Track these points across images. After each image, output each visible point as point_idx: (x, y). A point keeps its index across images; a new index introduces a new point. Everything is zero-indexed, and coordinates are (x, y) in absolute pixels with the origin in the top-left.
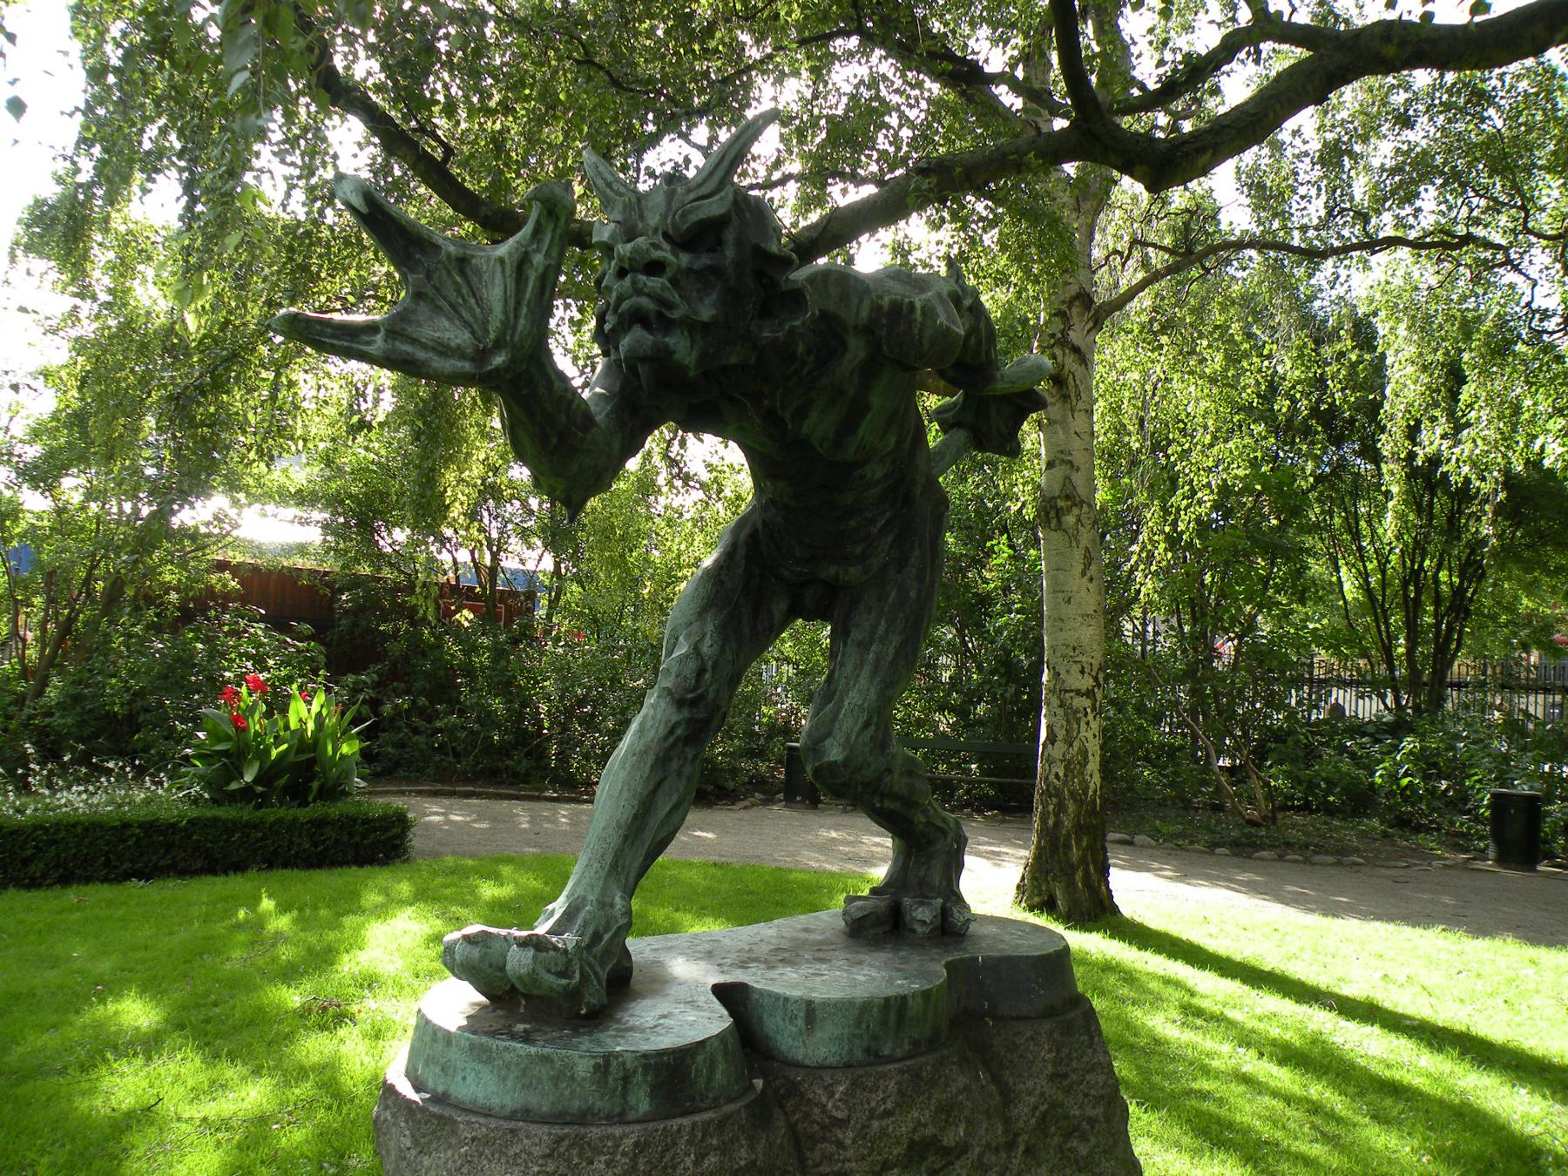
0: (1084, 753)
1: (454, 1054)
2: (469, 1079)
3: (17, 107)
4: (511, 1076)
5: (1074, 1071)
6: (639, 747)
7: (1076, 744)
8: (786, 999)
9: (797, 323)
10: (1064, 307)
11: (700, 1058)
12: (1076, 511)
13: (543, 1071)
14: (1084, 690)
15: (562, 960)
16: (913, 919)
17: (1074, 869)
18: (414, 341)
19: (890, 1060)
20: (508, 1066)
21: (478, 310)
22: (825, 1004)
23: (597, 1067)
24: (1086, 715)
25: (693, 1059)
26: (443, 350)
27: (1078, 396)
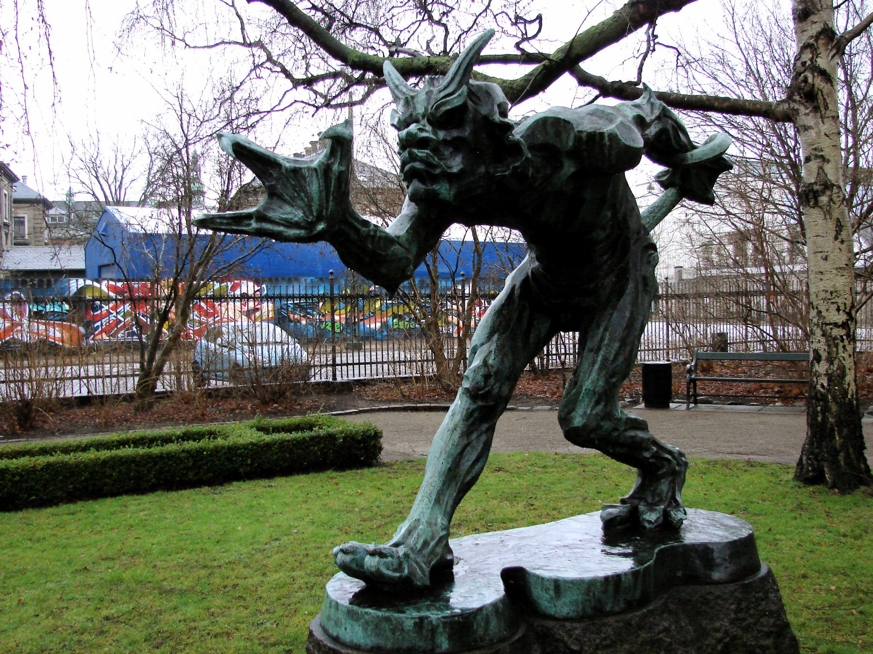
0: (842, 369)
1: (341, 615)
2: (348, 630)
4: (369, 628)
5: (752, 616)
6: (451, 426)
7: (836, 362)
8: (543, 579)
9: (518, 164)
10: (812, 41)
11: (479, 617)
12: (828, 193)
13: (386, 626)
14: (840, 323)
15: (396, 562)
16: (644, 519)
17: (837, 452)
19: (612, 613)
20: (367, 623)
22: (566, 581)
23: (415, 623)
24: (842, 341)
25: (474, 618)
26: (290, 224)
27: (826, 107)
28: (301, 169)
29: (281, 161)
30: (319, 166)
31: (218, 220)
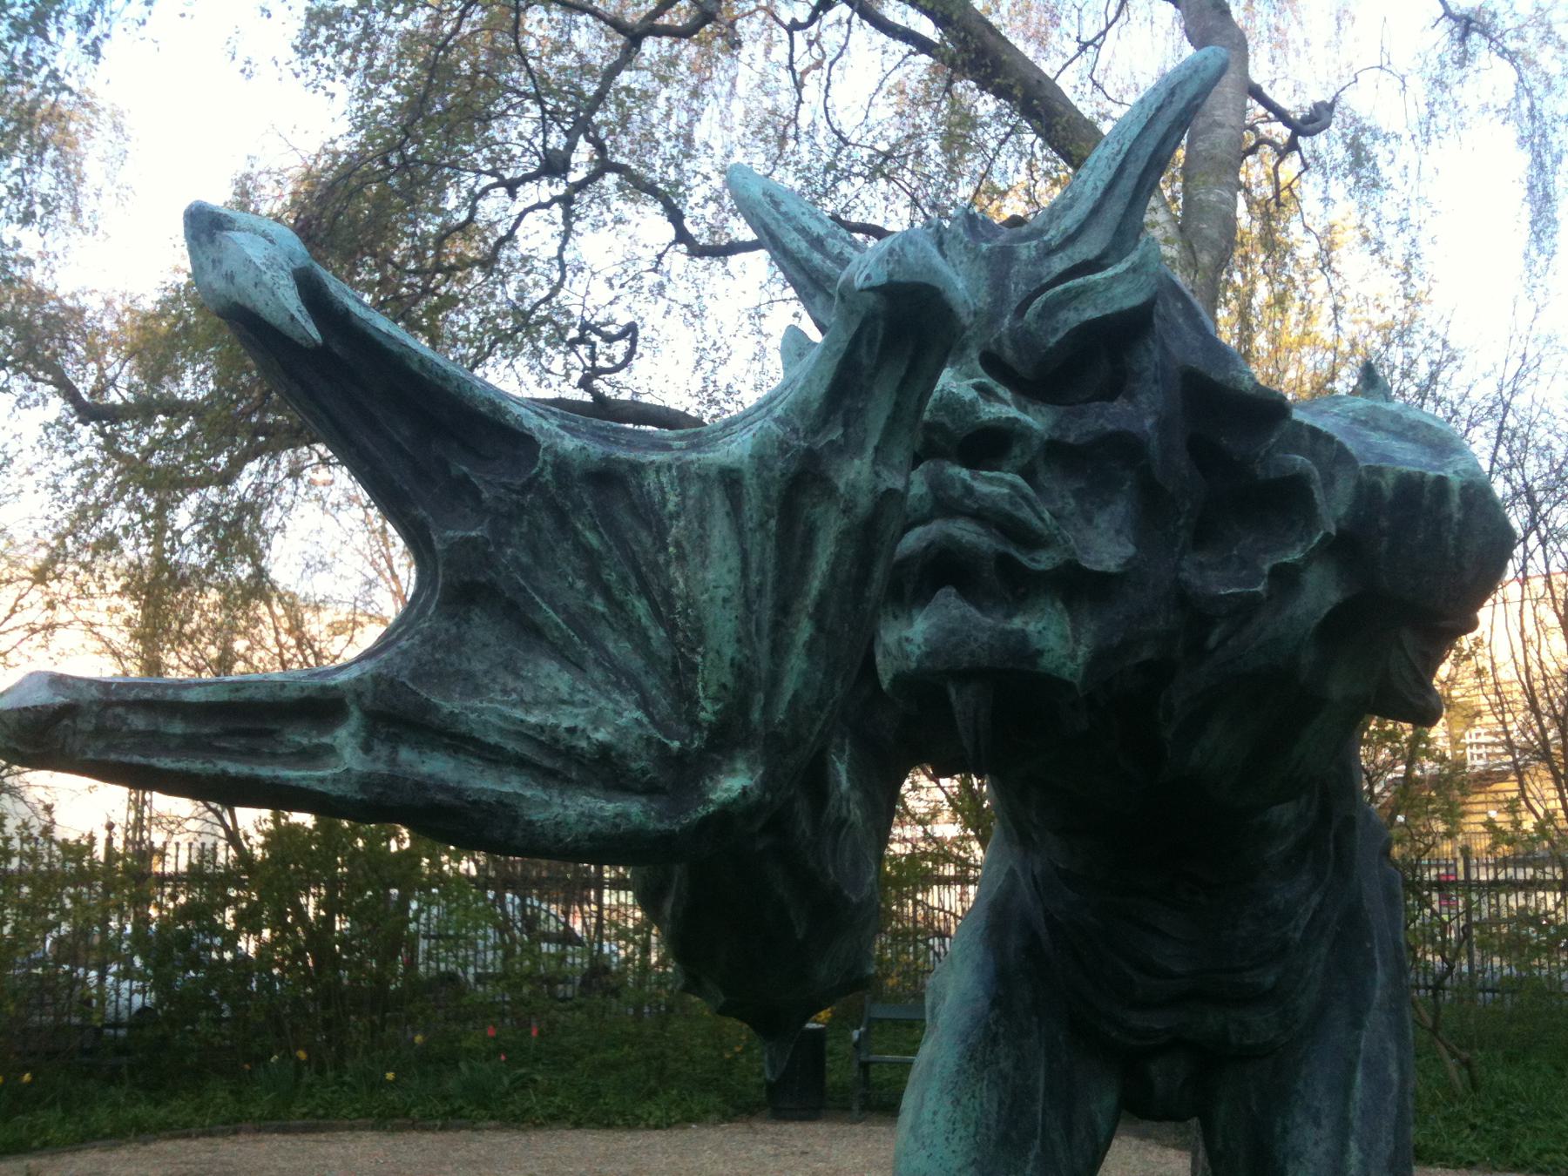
3: (183, 15)
18: (459, 742)
21: (657, 634)
26: (559, 761)
28: (637, 468)
29: (532, 422)
30: (760, 459)
31: (139, 722)
